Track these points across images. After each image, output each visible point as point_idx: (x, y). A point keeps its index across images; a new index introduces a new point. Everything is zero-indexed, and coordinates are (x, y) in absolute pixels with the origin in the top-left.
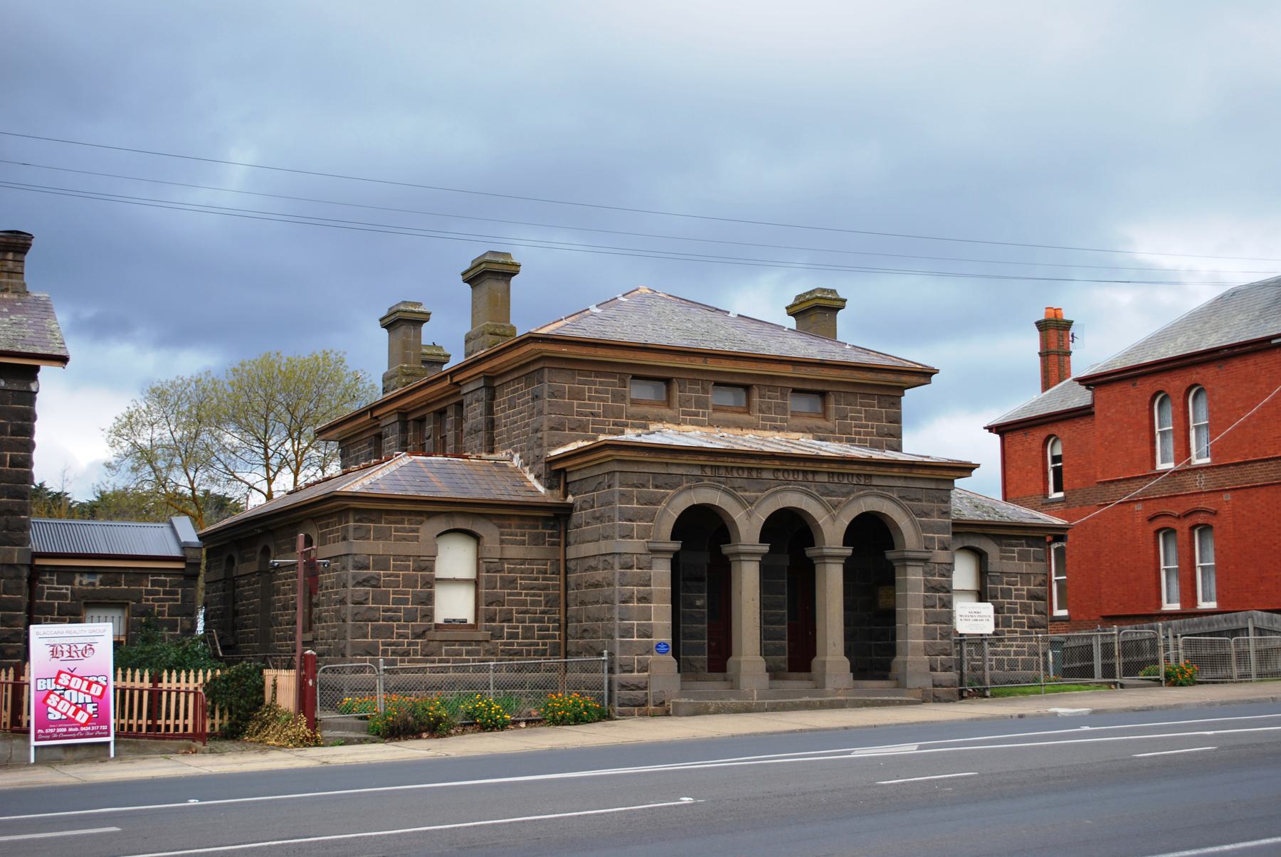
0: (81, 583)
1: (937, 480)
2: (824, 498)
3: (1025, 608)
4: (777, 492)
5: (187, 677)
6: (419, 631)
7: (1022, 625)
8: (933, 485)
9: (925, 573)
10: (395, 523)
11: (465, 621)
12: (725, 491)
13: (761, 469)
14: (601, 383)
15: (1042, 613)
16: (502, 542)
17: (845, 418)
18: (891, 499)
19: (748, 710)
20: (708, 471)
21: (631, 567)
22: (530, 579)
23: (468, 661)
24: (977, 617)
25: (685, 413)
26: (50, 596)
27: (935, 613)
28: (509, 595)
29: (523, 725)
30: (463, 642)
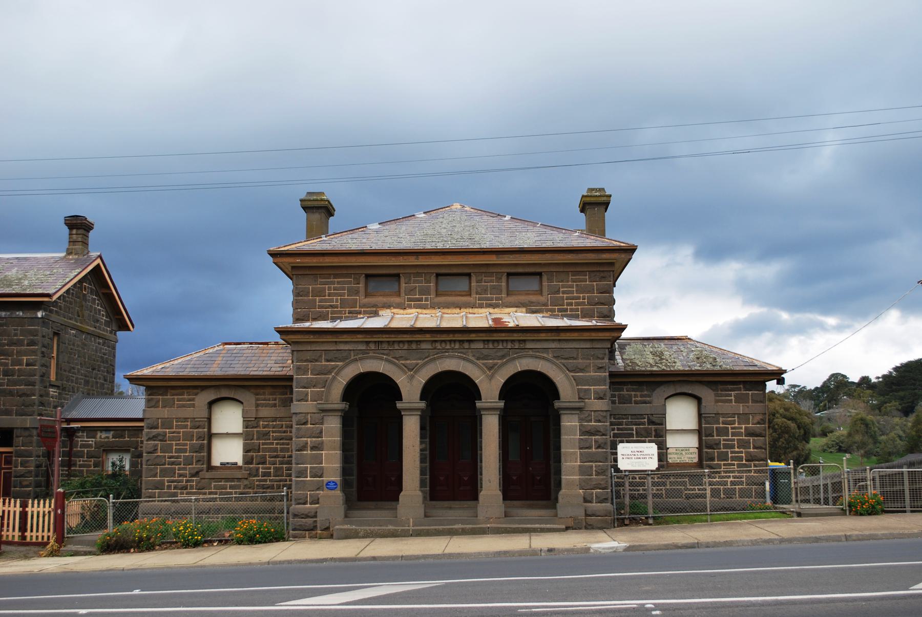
0: (100, 437)
1: (592, 340)
2: (479, 362)
3: (743, 444)
4: (435, 359)
5: (44, 504)
6: (194, 471)
7: (741, 459)
8: (588, 345)
9: (581, 420)
10: (177, 395)
11: (236, 464)
12: (387, 360)
13: (420, 341)
14: (338, 283)
15: (761, 448)
16: (257, 406)
17: (558, 292)
18: (544, 358)
19: (482, 532)
20: (372, 346)
21: (305, 423)
22: (280, 432)
23: (231, 493)
24: (642, 456)
25: (410, 300)
26: (83, 446)
27: (590, 453)
28: (263, 444)
29: (651, 521)
30: (227, 480)
